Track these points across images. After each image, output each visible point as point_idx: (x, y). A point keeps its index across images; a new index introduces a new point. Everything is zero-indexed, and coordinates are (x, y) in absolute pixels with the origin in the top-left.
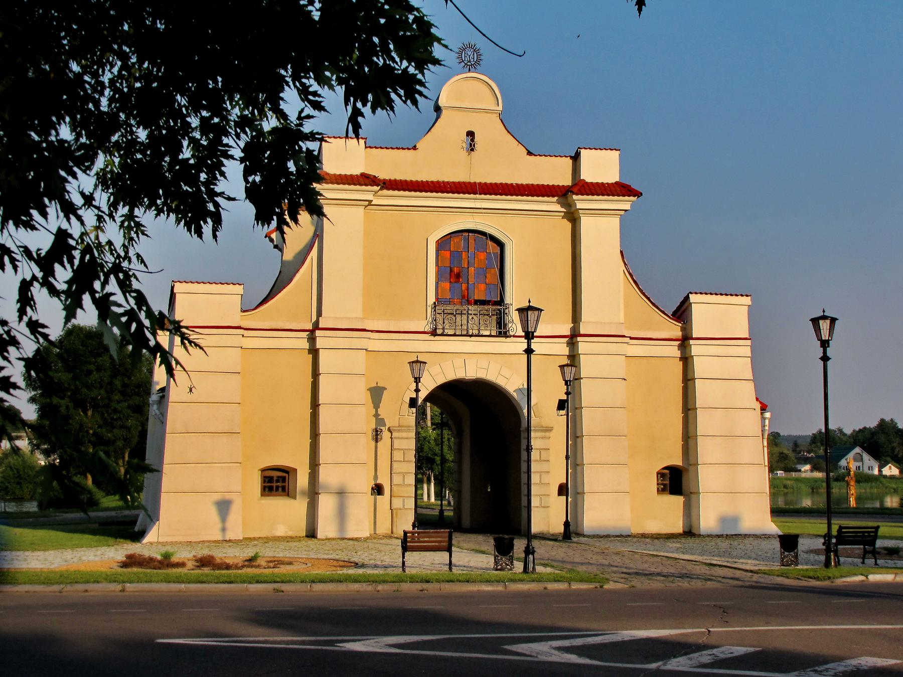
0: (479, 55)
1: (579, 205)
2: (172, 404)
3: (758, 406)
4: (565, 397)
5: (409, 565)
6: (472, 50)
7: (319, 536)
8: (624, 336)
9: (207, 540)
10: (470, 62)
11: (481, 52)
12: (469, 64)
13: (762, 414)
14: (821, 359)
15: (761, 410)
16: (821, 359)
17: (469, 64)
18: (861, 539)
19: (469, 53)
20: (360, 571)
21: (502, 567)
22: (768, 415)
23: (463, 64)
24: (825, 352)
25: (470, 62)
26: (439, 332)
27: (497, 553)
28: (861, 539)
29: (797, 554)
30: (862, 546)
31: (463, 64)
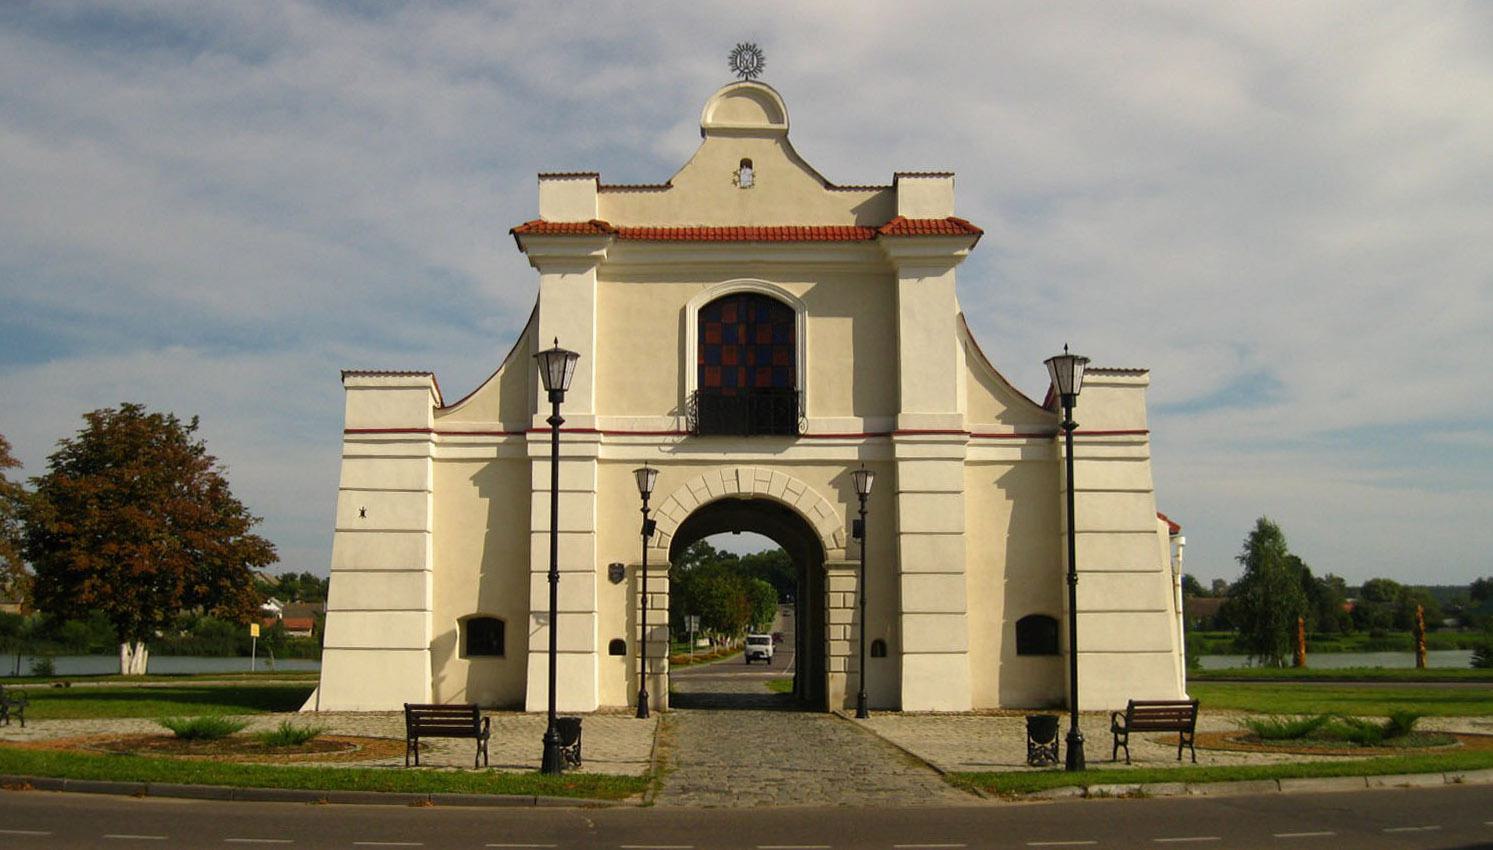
0: (760, 60)
1: (893, 253)
2: (545, 488)
3: (1163, 528)
4: (859, 517)
5: (1092, 759)
6: (751, 53)
7: (906, 707)
8: (962, 433)
9: (582, 710)
10: (747, 68)
11: (763, 55)
12: (746, 71)
13: (1172, 539)
14: (642, 510)
15: (1171, 534)
16: (642, 510)
17: (746, 71)
18: (472, 726)
19: (747, 57)
20: (315, 763)
21: (1041, 760)
22: (1183, 540)
23: (738, 72)
24: (645, 504)
25: (747, 68)
26: (1052, 362)
27: (1032, 741)
28: (472, 726)
29: (1057, 747)
30: (1178, 733)
31: (738, 72)
